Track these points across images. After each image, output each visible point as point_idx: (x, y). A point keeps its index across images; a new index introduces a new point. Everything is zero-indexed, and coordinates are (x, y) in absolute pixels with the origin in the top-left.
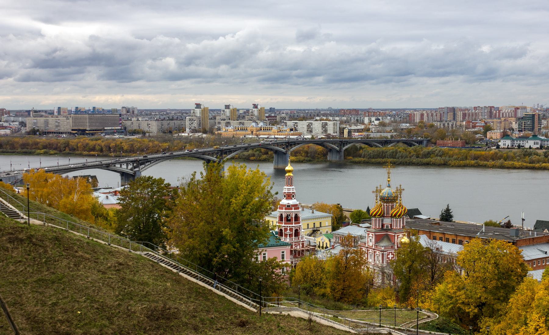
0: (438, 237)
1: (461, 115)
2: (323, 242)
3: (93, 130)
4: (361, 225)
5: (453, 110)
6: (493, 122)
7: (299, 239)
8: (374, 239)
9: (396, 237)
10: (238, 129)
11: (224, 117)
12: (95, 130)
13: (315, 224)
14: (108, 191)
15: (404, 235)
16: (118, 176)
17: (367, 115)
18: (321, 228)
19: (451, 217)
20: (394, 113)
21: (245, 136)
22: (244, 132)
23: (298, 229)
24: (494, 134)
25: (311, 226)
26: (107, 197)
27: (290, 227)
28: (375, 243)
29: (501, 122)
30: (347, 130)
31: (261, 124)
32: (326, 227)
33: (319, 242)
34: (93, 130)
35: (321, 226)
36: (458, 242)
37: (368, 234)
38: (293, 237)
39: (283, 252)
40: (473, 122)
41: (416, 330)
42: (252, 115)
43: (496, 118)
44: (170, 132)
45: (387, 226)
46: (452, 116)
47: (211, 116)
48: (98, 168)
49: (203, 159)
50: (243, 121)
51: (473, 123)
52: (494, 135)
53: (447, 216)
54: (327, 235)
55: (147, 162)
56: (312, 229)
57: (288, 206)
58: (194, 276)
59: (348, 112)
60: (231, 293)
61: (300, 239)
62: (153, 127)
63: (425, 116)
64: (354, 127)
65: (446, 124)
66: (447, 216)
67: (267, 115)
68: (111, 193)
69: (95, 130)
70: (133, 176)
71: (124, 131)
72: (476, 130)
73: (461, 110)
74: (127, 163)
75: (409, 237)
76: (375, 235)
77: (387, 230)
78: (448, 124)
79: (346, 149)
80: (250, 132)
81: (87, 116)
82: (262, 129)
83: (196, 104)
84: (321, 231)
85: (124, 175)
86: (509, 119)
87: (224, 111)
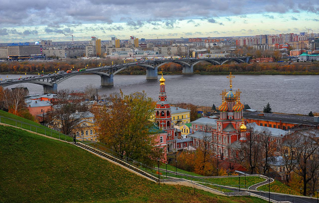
0: (264, 124)
1: (271, 40)
2: (185, 129)
3: (23, 57)
4: (210, 117)
5: (266, 36)
6: (293, 44)
7: (170, 128)
8: (222, 126)
9: (237, 125)
10: (121, 53)
11: (111, 46)
12: (24, 57)
13: (175, 117)
14: (35, 98)
15: (242, 123)
16: (42, 87)
17: (207, 41)
18: (183, 119)
19: (270, 109)
20: (225, 40)
21: (126, 58)
22: (125, 56)
23: (169, 121)
24: (294, 52)
25: (176, 118)
26: (36, 102)
27: (164, 119)
28: (223, 129)
29: (299, 44)
30: (195, 52)
31: (136, 50)
32: (186, 119)
33: (182, 129)
34: (23, 57)
35: (183, 118)
36: (278, 127)
37: (218, 123)
38: (166, 126)
39: (161, 137)
40: (280, 44)
41: (270, 192)
42: (130, 44)
43: (295, 41)
44: (76, 57)
45: (231, 118)
46: (265, 41)
47: (102, 46)
48: (28, 82)
49: (99, 74)
50: (124, 48)
51: (280, 45)
52: (295, 53)
53: (268, 110)
54: (187, 124)
55: (61, 77)
56: (177, 121)
57: (162, 105)
58: (103, 155)
59: (194, 40)
60: (127, 165)
61: (171, 127)
62: (63, 54)
63: (246, 41)
64: (199, 50)
65: (262, 46)
66: (268, 110)
67: (140, 44)
68: (39, 99)
69: (24, 57)
70: (52, 87)
71: (43, 57)
72: (282, 50)
73: (270, 36)
74: (48, 78)
75: (246, 125)
76: (222, 124)
77: (230, 121)
78: (263, 47)
79: (194, 66)
80: (129, 56)
81: (18, 47)
82: (137, 53)
83: (92, 37)
84: (183, 121)
85: (45, 86)
86: (304, 41)
87: (111, 41)
